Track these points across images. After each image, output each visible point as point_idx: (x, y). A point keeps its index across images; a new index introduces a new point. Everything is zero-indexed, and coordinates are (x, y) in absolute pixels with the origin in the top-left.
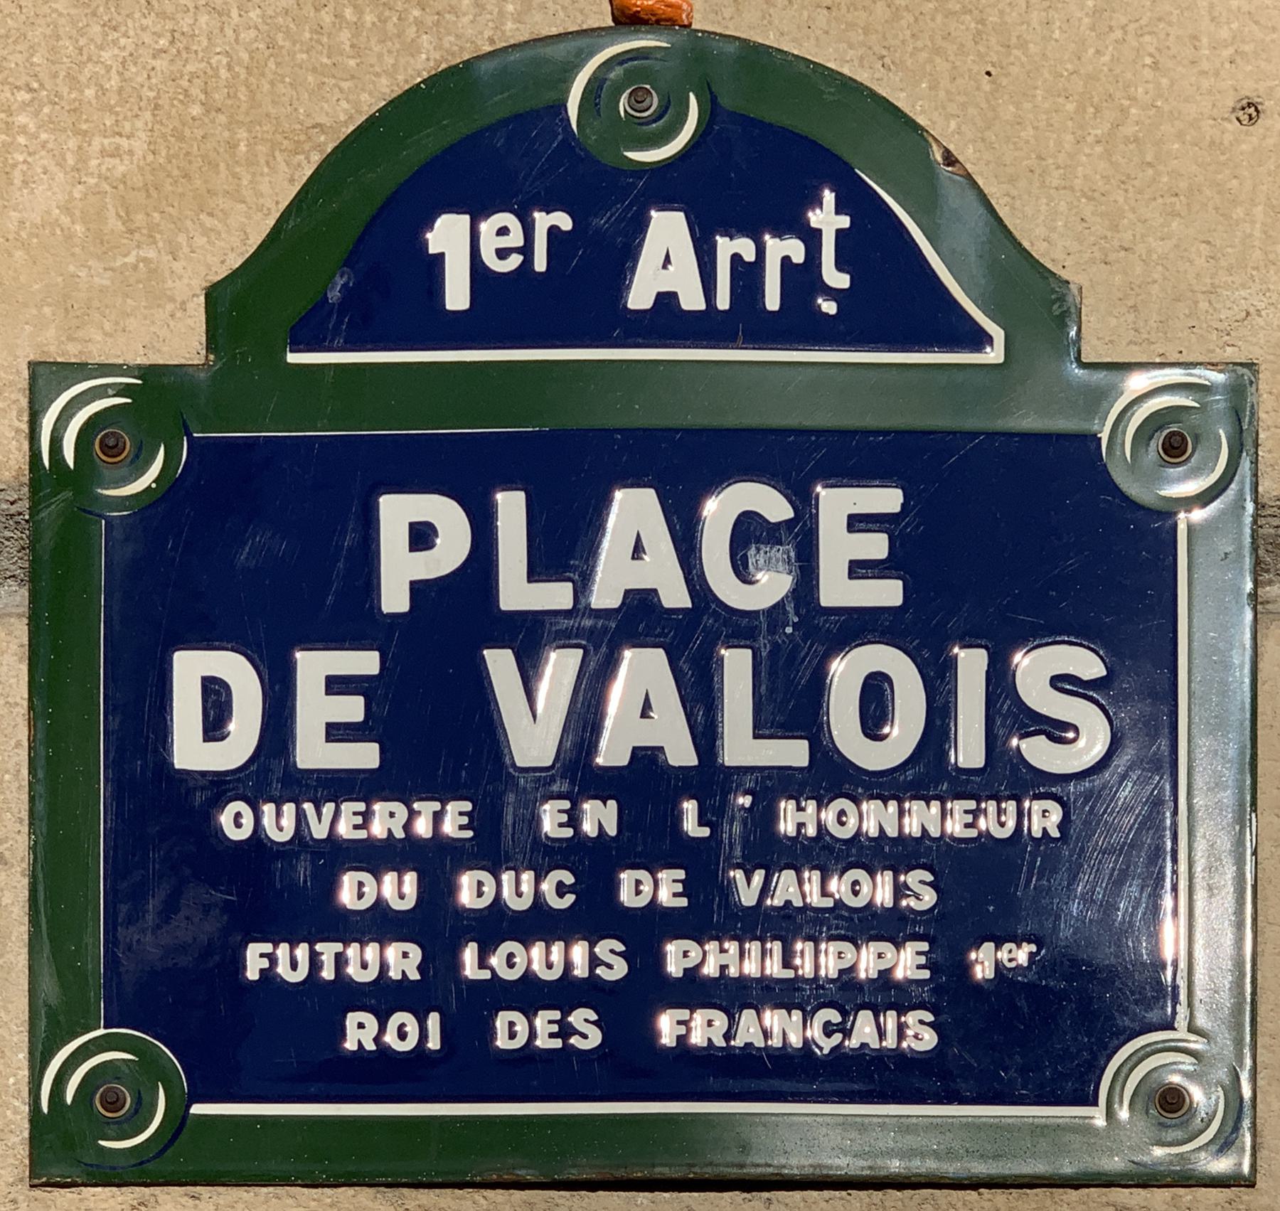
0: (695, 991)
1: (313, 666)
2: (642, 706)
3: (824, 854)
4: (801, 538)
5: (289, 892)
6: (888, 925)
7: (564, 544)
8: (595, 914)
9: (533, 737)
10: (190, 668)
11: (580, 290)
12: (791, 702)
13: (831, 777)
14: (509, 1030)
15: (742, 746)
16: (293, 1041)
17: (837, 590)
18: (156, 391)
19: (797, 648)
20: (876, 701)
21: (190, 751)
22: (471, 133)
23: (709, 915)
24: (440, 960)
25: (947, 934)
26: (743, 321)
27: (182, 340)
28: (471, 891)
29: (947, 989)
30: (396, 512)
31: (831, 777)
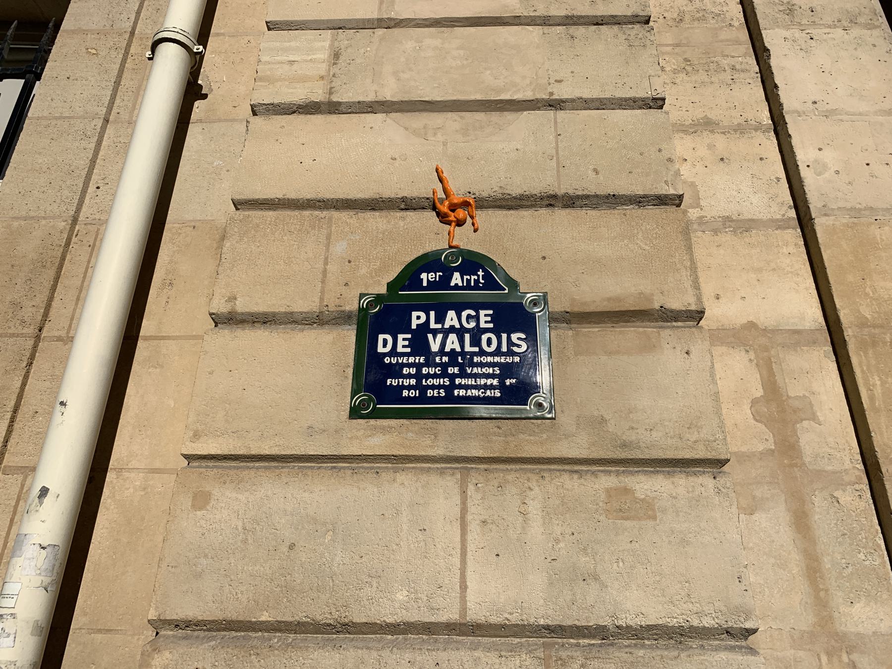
0: (460, 387)
1: (400, 337)
2: (453, 342)
3: (481, 365)
4: (477, 318)
5: (395, 371)
6: (492, 376)
7: (440, 319)
8: (444, 374)
9: (435, 347)
10: (381, 337)
11: (444, 283)
12: (476, 342)
13: (482, 353)
14: (430, 393)
16: (395, 395)
17: (483, 325)
18: (379, 298)
21: (381, 349)
22: (429, 262)
23: (463, 374)
24: (419, 381)
25: (502, 377)
26: (468, 287)
27: (383, 290)
28: (425, 371)
29: (502, 386)
30: (415, 314)
31: (482, 353)
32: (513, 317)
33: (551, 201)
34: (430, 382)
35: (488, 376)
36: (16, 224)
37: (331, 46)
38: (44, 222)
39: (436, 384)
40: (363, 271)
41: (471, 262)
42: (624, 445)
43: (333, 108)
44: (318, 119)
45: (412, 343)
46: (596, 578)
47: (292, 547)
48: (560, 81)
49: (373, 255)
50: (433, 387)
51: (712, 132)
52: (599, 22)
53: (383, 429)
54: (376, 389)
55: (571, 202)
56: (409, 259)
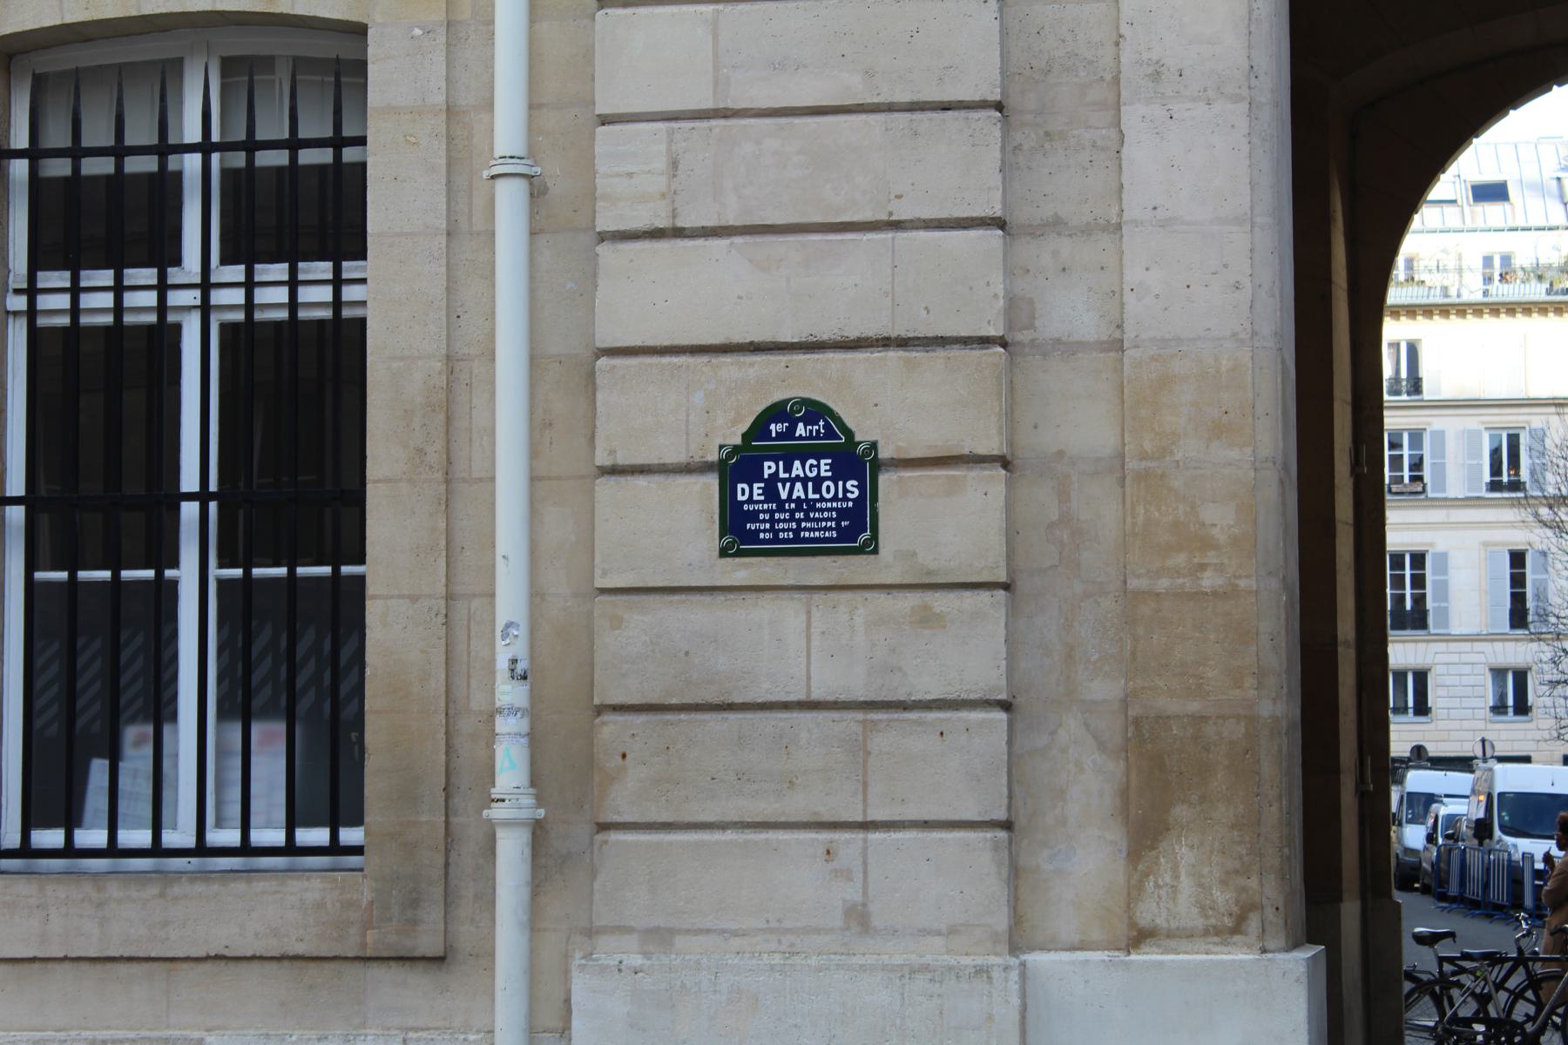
0: (805, 529)
1: (756, 486)
2: (799, 491)
3: (822, 510)
4: (818, 466)
5: (753, 516)
6: (831, 519)
7: (788, 469)
8: (792, 519)
9: (784, 495)
10: (740, 486)
11: (789, 434)
12: (817, 490)
13: (822, 499)
14: (781, 535)
15: (811, 496)
16: (753, 537)
17: (823, 474)
18: (735, 447)
19: (818, 481)
20: (828, 488)
21: (740, 498)
22: (777, 412)
23: (807, 519)
24: (772, 526)
25: (838, 521)
26: (811, 437)
27: (738, 441)
28: (777, 516)
29: (838, 528)
30: (766, 464)
31: (822, 499)
32: (854, 461)
33: (886, 343)
34: (781, 526)
35: (826, 529)
36: (395, 365)
37: (669, 150)
38: (420, 363)
39: (786, 529)
40: (720, 421)
41: (815, 411)
42: (929, 573)
43: (678, 233)
44: (662, 246)
45: (765, 491)
46: (900, 669)
47: (687, 653)
48: (899, 197)
49: (722, 409)
50: (783, 530)
51: (1059, 234)
52: (946, 107)
53: (746, 566)
54: (738, 531)
55: (903, 343)
56: (760, 409)
